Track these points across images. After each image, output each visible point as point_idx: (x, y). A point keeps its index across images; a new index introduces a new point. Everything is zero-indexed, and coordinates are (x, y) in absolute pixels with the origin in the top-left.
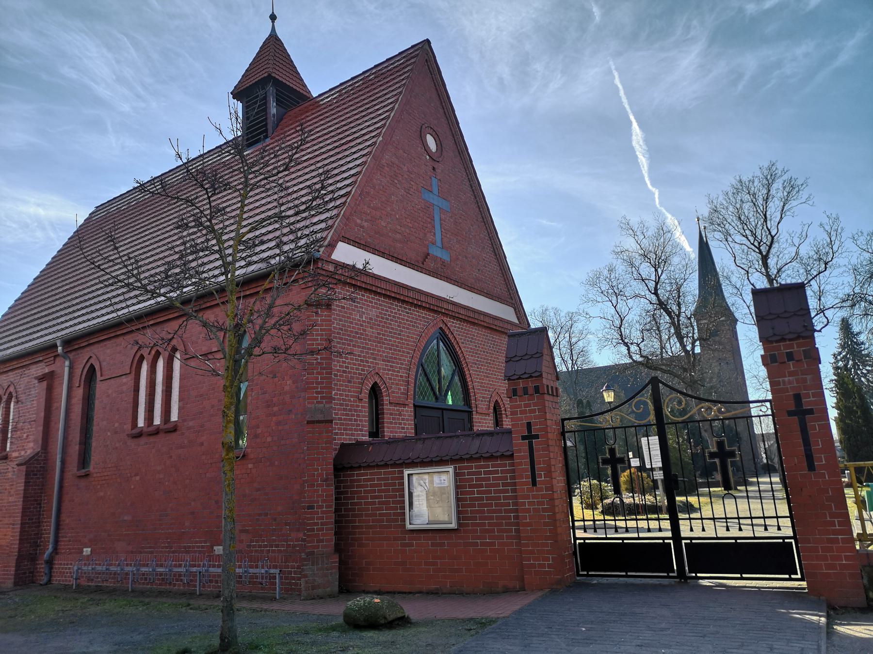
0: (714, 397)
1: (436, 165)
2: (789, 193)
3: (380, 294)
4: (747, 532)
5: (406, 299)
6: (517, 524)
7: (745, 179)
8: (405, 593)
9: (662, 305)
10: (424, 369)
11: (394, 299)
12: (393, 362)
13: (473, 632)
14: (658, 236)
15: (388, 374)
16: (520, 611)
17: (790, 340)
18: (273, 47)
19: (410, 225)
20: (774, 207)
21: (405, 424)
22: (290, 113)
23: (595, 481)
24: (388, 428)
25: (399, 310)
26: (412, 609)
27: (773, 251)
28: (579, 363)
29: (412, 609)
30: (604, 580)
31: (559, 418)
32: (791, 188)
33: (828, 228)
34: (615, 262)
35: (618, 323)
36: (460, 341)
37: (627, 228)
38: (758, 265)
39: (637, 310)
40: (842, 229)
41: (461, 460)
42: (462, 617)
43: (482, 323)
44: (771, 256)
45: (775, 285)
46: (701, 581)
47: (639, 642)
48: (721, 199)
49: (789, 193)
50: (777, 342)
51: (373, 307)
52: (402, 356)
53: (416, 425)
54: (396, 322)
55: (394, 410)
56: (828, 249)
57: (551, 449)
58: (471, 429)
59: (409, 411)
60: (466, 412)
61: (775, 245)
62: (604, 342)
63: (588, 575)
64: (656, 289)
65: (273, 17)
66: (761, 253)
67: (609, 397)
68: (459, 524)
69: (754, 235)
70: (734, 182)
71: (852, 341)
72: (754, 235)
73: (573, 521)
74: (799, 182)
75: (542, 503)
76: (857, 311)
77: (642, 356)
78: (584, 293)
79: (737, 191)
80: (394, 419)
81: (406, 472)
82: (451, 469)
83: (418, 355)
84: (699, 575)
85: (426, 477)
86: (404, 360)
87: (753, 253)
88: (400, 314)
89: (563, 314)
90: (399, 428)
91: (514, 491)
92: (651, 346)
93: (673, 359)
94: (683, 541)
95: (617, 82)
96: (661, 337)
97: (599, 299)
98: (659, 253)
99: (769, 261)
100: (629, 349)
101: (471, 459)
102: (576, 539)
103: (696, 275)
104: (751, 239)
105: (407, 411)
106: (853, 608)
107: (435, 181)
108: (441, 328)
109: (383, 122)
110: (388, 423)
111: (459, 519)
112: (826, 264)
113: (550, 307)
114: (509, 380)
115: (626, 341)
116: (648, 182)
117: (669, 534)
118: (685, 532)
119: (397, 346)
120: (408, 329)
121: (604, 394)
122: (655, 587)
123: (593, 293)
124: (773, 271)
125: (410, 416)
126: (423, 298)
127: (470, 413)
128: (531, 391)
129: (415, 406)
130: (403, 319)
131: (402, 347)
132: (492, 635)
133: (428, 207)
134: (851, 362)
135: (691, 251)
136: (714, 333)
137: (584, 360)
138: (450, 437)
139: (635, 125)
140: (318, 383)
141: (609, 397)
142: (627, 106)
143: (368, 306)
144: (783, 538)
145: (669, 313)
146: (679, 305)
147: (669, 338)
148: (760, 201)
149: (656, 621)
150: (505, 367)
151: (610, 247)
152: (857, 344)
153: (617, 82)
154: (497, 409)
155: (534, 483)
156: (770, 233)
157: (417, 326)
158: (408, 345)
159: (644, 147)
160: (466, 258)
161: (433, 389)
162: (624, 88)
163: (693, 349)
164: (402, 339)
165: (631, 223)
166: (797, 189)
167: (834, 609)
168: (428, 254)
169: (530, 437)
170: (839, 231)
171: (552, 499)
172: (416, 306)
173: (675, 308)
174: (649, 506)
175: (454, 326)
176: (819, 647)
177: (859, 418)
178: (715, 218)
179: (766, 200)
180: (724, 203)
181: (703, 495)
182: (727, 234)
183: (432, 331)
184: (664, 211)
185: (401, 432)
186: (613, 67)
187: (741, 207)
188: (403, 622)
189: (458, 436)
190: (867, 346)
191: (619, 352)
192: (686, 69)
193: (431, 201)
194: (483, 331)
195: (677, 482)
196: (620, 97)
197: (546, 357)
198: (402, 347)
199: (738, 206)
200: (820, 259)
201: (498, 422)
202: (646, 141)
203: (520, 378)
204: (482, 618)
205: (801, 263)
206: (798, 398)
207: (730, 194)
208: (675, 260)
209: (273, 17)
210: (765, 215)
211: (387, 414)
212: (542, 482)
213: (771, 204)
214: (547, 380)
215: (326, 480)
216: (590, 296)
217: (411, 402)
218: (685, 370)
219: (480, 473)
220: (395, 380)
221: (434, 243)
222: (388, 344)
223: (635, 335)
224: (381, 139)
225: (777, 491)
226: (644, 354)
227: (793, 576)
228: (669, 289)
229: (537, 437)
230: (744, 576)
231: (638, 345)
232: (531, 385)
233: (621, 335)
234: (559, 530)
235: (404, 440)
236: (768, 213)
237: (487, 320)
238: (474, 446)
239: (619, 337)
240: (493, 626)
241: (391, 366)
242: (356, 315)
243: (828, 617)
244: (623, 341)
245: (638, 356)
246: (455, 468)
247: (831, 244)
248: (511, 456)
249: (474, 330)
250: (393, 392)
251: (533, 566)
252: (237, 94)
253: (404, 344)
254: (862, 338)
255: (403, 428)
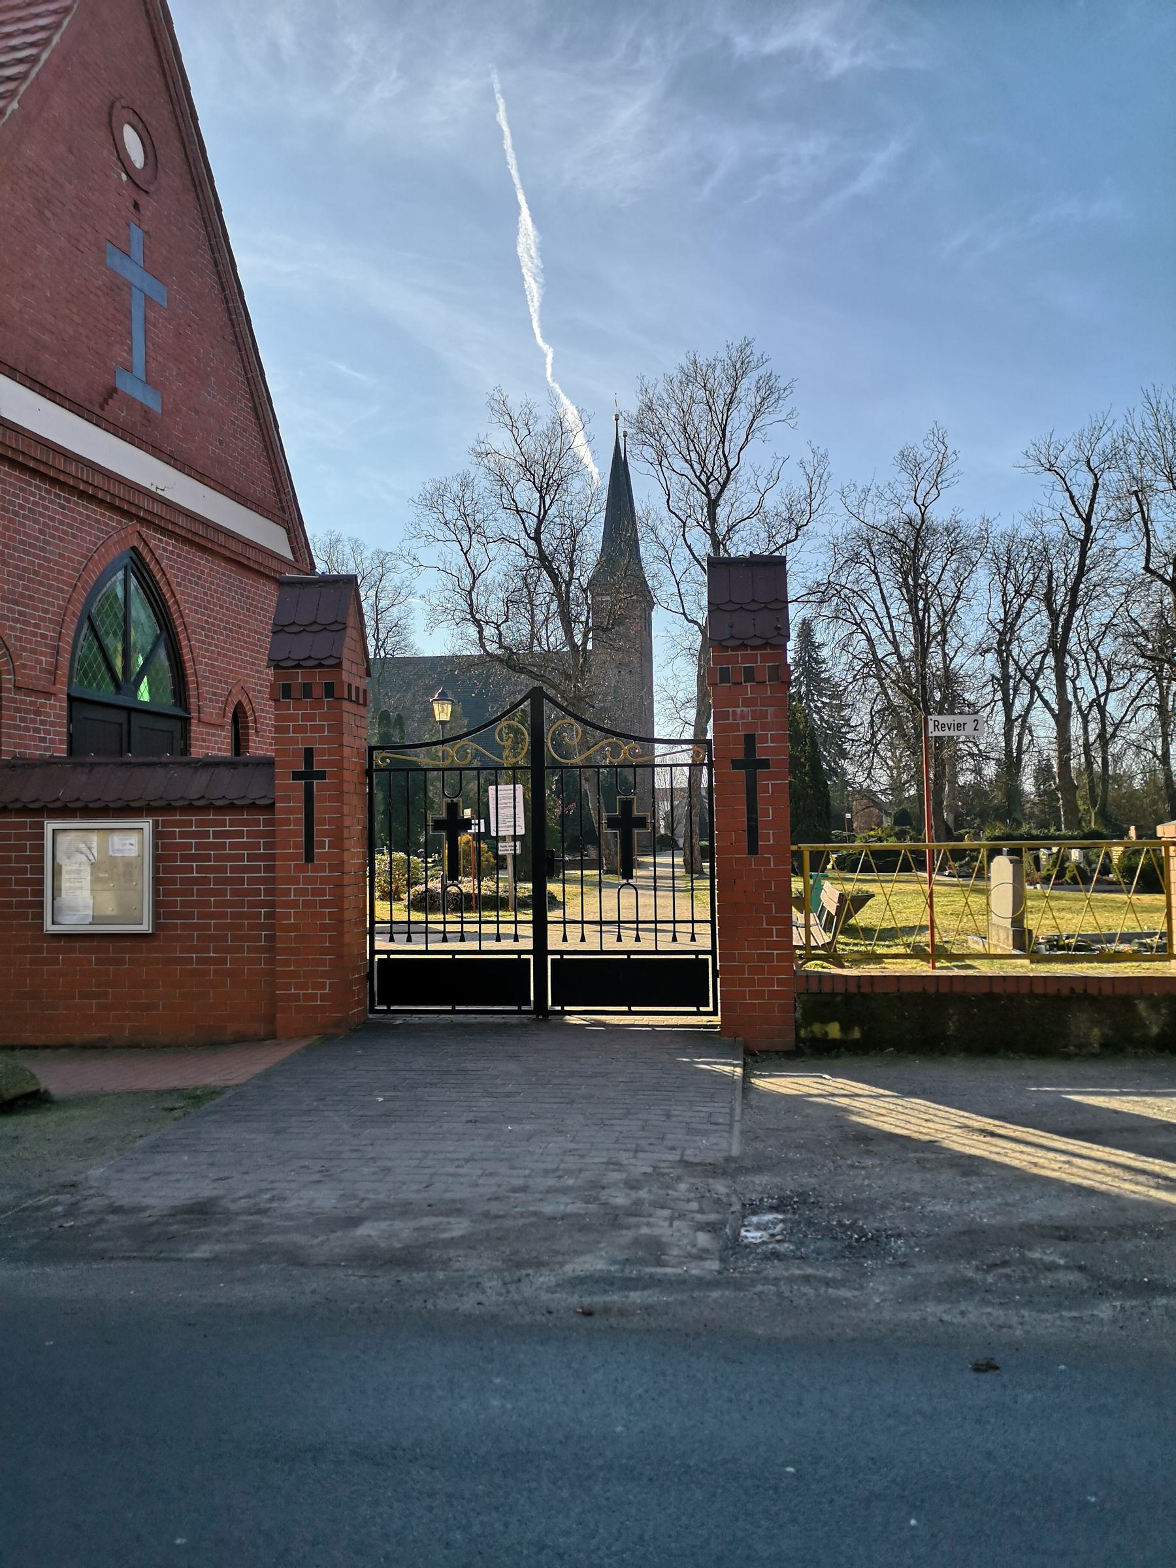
0: (607, 724)
1: (143, 200)
2: (764, 399)
4: (647, 943)
5: (61, 478)
6: (272, 927)
7: (701, 361)
8: (36, 1047)
9: (545, 561)
10: (93, 628)
11: (34, 472)
12: (26, 606)
13: (176, 1113)
14: (551, 436)
16: (267, 1075)
17: (754, 648)
19: (77, 319)
20: (739, 417)
21: (47, 732)
23: (402, 854)
24: (10, 736)
25: (42, 498)
26: (53, 1076)
27: (727, 494)
28: (389, 647)
29: (53, 1076)
30: (415, 1019)
31: (365, 745)
32: (768, 393)
33: (810, 470)
34: (473, 471)
35: (467, 582)
36: (173, 581)
37: (502, 410)
38: (701, 515)
39: (502, 564)
40: (829, 475)
41: (169, 808)
42: (156, 1086)
43: (222, 551)
44: (722, 502)
45: (722, 553)
46: (568, 1017)
47: (471, 1116)
48: (660, 388)
49: (764, 399)
50: (734, 649)
52: (46, 594)
53: (70, 736)
54: (36, 521)
55: (23, 702)
56: (804, 505)
57: (346, 798)
58: (186, 751)
59: (56, 708)
60: (177, 719)
61: (731, 485)
62: (439, 613)
63: (389, 1011)
64: (538, 531)
66: (708, 494)
67: (442, 712)
68: (156, 925)
69: (703, 462)
70: (684, 362)
71: (811, 656)
72: (703, 462)
73: (373, 922)
74: (782, 384)
75: (321, 892)
76: (826, 610)
77: (501, 646)
78: (413, 519)
79: (688, 380)
80: (23, 720)
81: (50, 826)
82: (147, 825)
83: (81, 595)
84: (566, 1008)
85: (94, 838)
86: (52, 604)
87: (697, 493)
88: (46, 508)
89: (367, 553)
90: (33, 739)
91: (269, 869)
92: (518, 631)
93: (548, 655)
94: (550, 957)
95: (502, 118)
96: (533, 616)
97: (439, 535)
98: (550, 466)
99: (718, 510)
100: (480, 632)
101: (190, 808)
102: (373, 952)
103: (601, 518)
104: (697, 467)
105: (53, 707)
106: (777, 1052)
107: (136, 234)
108: (134, 549)
109: (20, 68)
110: (9, 727)
111: (156, 916)
112: (798, 529)
113: (344, 537)
114: (277, 667)
115: (478, 616)
116: (537, 331)
117: (528, 944)
118: (554, 941)
119: (36, 573)
120: (61, 539)
121: (436, 706)
122: (498, 1029)
123: (431, 521)
124: (722, 529)
125: (57, 716)
126: (98, 481)
127: (186, 721)
128: (318, 692)
129: (71, 699)
130: (53, 519)
131: (46, 577)
132: (214, 1117)
133: (117, 288)
134: (803, 689)
135: (598, 473)
136: (619, 621)
137: (398, 642)
138: (148, 765)
139: (525, 213)
141: (442, 712)
142: (514, 173)
144: (697, 953)
145: (554, 576)
146: (572, 565)
147: (547, 619)
148: (720, 405)
149: (498, 1081)
150: (271, 644)
151: (469, 444)
152: (817, 662)
153: (502, 118)
154: (239, 718)
155: (309, 857)
156: (726, 463)
157: (98, 534)
158: (60, 572)
159: (537, 261)
160: (197, 412)
161: (110, 668)
162: (513, 135)
163: (585, 643)
164: (48, 560)
165: (509, 402)
166: (776, 395)
167: (753, 1054)
168: (115, 390)
169: (308, 775)
170: (825, 478)
171: (339, 885)
172: (83, 495)
173: (564, 569)
174: (486, 897)
175: (162, 548)
176: (732, 1109)
177: (806, 774)
178: (647, 424)
179: (729, 405)
180: (665, 396)
181: (572, 881)
182: (662, 453)
183: (116, 551)
184: (560, 391)
185: (37, 748)
186: (497, 87)
187: (690, 408)
188: (36, 1100)
189: (165, 765)
190: (830, 665)
191: (464, 636)
192: (623, 128)
193: (127, 275)
194: (221, 567)
195: (540, 860)
196: (504, 151)
197: (351, 633)
198: (46, 577)
199: (685, 408)
200: (791, 520)
201: (239, 744)
202: (542, 249)
203: (298, 666)
204: (196, 1089)
205: (763, 521)
206: (750, 740)
207: (676, 382)
208: (575, 484)
210: (724, 431)
211: (9, 708)
212: (324, 856)
213: (734, 414)
214: (350, 675)
216: (424, 526)
217: (62, 689)
218: (568, 677)
219: (206, 834)
220: (28, 641)
221: (129, 369)
222: (17, 567)
223: (494, 607)
224: (15, 105)
225: (662, 878)
226: (507, 642)
227: (702, 1009)
228: (558, 534)
229: (322, 775)
230: (633, 1009)
231: (498, 627)
232: (319, 680)
233: (471, 605)
234: (347, 938)
235: (48, 763)
236: (728, 428)
237: (233, 545)
238: (197, 785)
239: (467, 608)
240: (217, 1101)
241: (21, 613)
243: (745, 1066)
244: (473, 616)
245: (496, 646)
246: (156, 824)
247: (810, 497)
248: (270, 808)
249: (204, 563)
250: (24, 666)
251: (296, 997)
253: (51, 570)
254: (825, 653)
255: (43, 740)
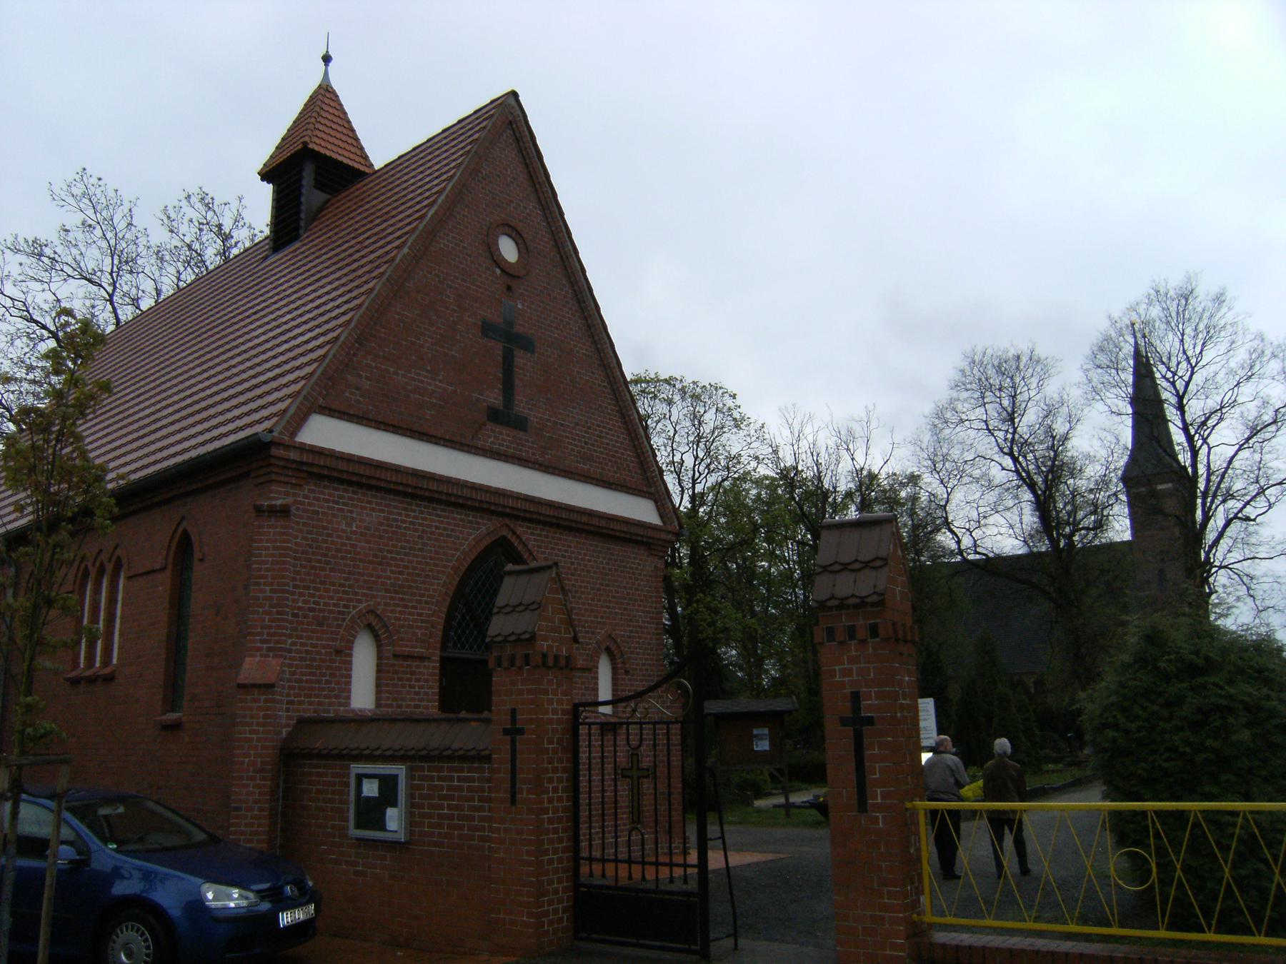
3: (388, 491)
11: (414, 496)
15: (392, 612)
18: (324, 104)
22: (335, 200)
43: (586, 527)
51: (372, 510)
65: (327, 59)
140: (263, 627)
143: (362, 508)
155: (513, 801)
164: (425, 557)
209: (327, 59)
215: (261, 771)
222: (397, 566)
242: (338, 523)
252: (266, 175)
